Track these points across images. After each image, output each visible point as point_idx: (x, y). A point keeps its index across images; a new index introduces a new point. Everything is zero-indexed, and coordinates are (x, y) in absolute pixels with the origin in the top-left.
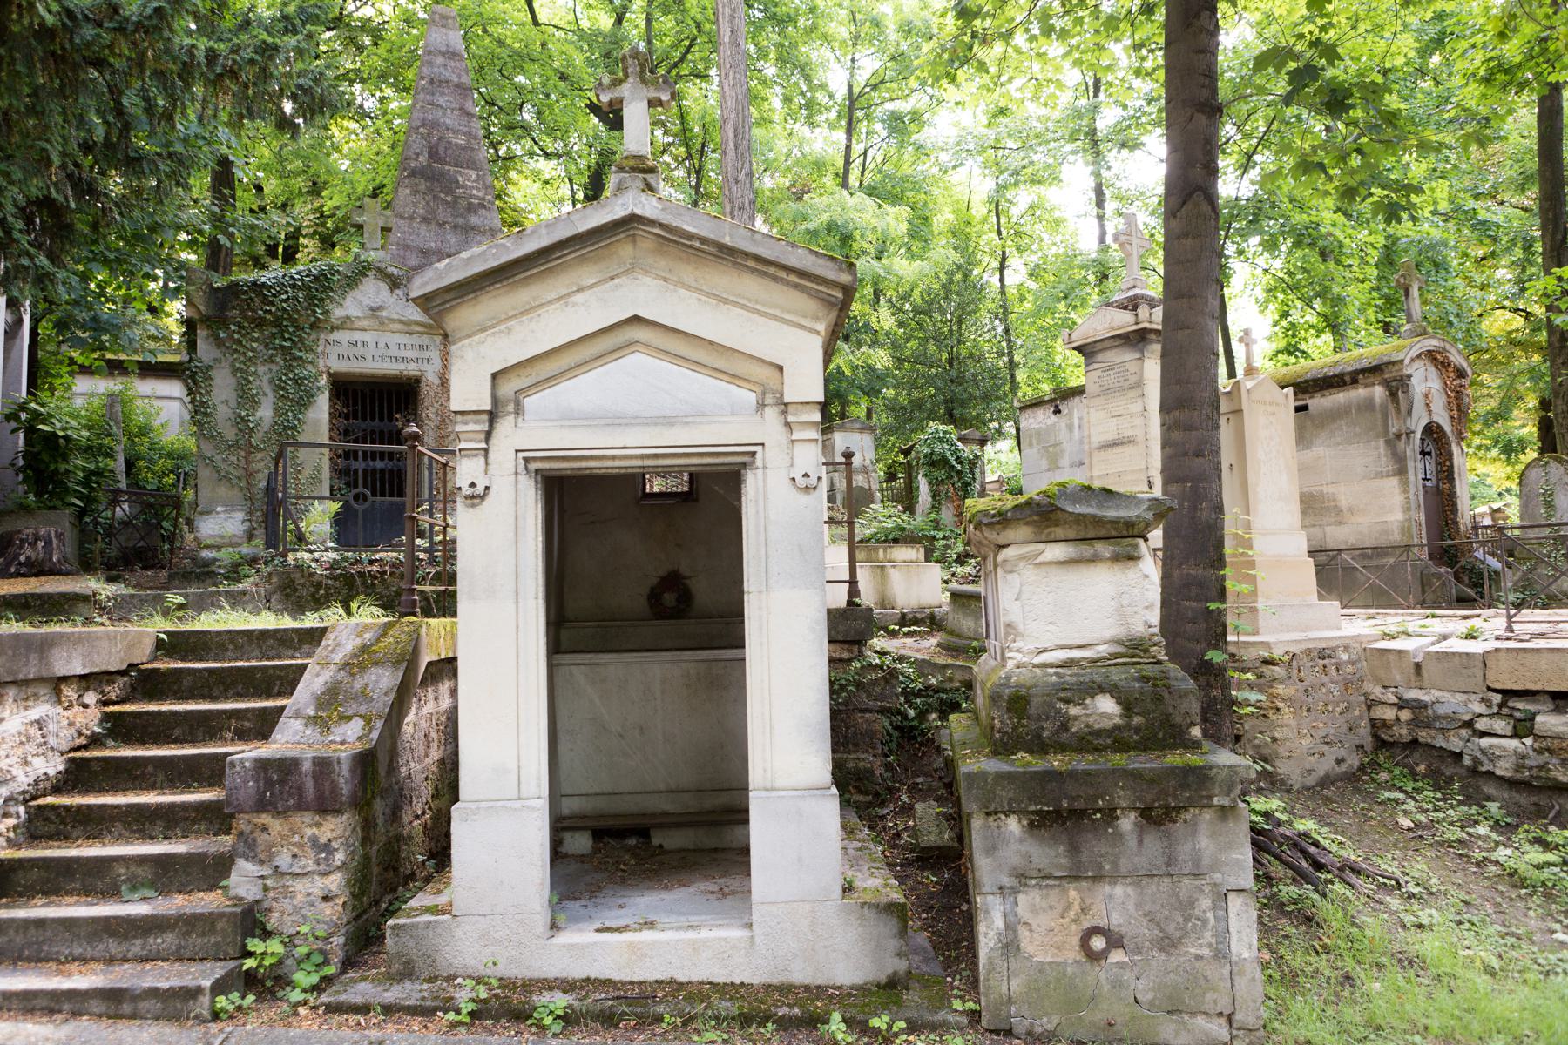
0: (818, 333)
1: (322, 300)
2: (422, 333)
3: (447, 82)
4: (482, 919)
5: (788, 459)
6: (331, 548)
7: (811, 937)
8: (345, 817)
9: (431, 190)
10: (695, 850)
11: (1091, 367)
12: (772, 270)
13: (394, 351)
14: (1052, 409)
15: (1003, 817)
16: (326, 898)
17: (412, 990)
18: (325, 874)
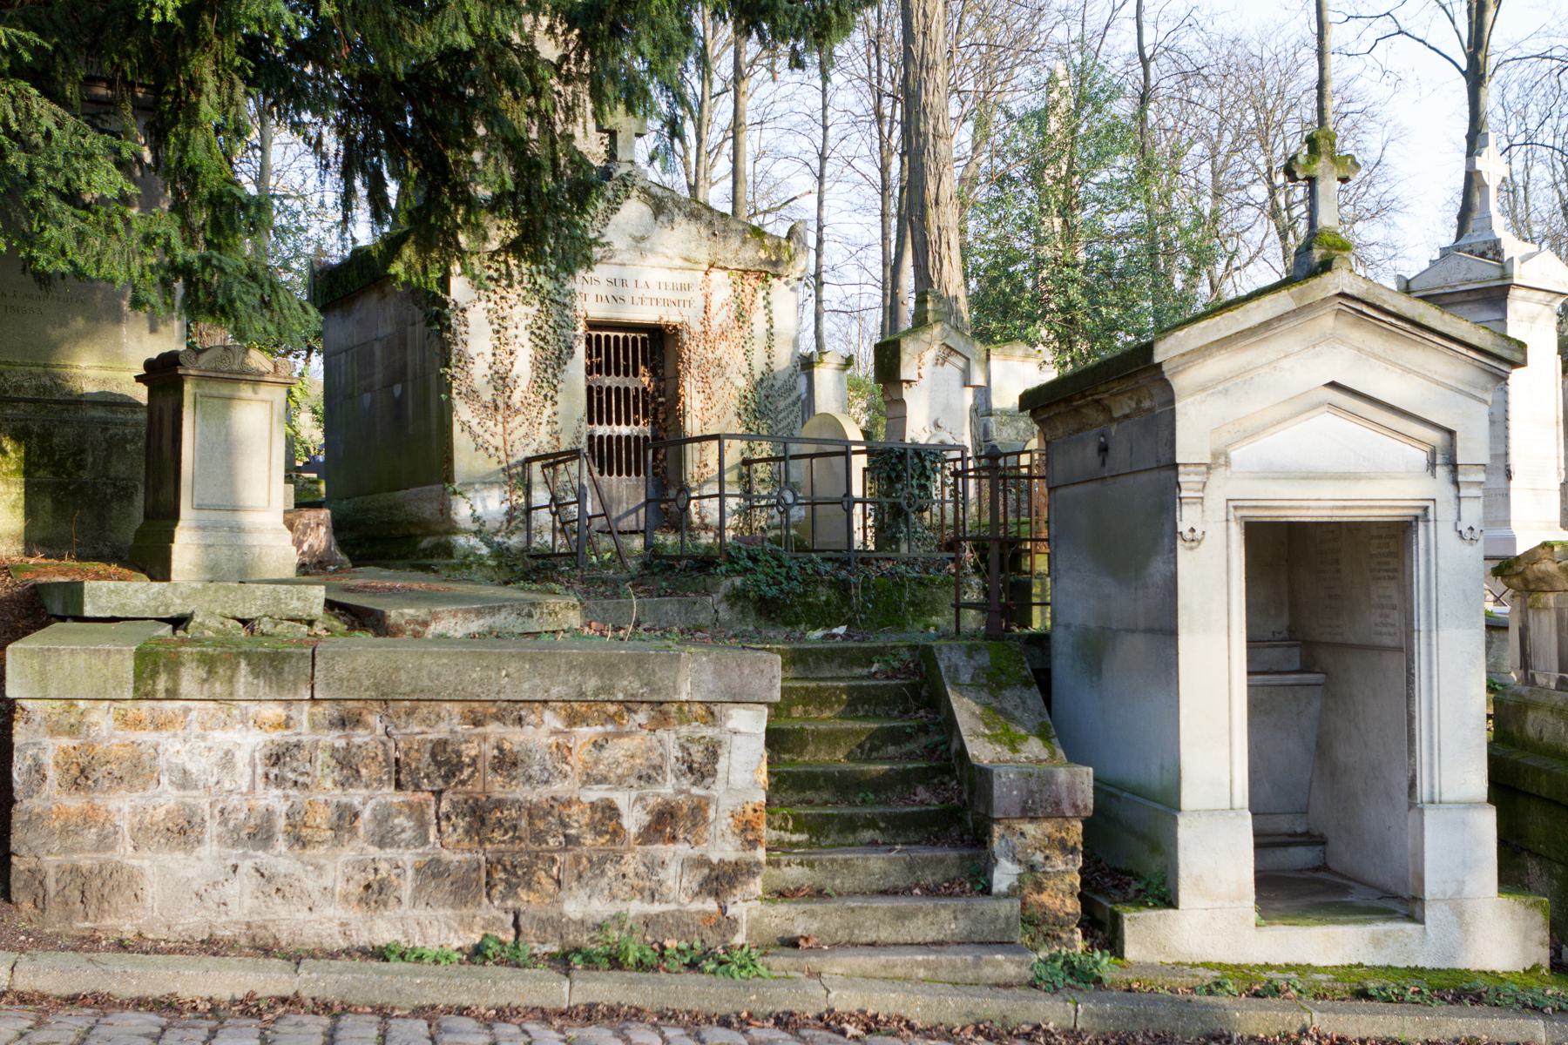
0: (1485, 402)
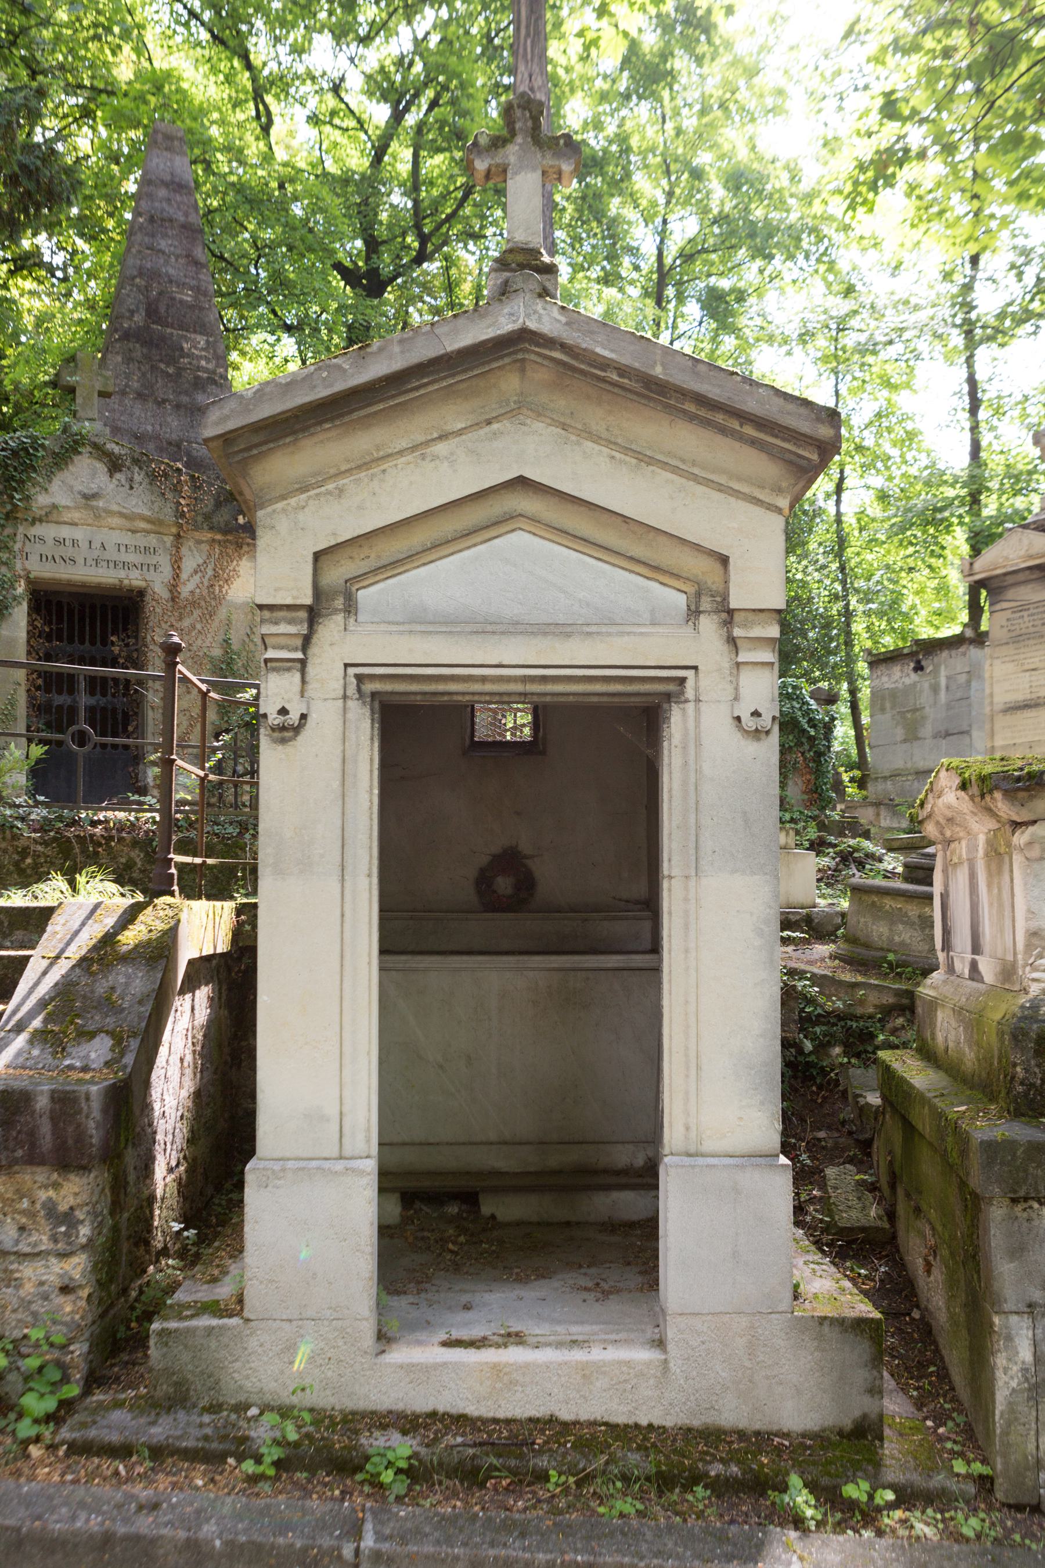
0: (779, 510)
1: (22, 482)
2: (148, 532)
3: (171, 220)
4: (286, 1326)
5: (730, 689)
6: (42, 803)
7: (748, 1364)
8: (92, 1175)
9: (148, 358)
10: (539, 1224)
11: (998, 607)
12: (720, 418)
13: (111, 554)
14: (912, 665)
15: (1036, 1205)
16: (65, 1290)
17: (188, 1424)
18: (63, 1255)
